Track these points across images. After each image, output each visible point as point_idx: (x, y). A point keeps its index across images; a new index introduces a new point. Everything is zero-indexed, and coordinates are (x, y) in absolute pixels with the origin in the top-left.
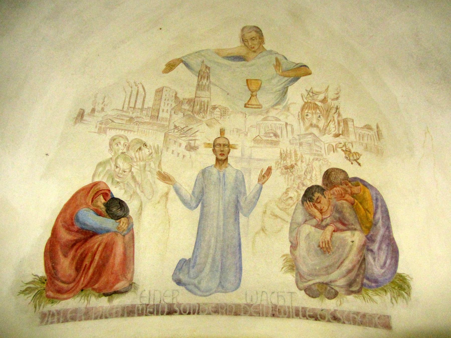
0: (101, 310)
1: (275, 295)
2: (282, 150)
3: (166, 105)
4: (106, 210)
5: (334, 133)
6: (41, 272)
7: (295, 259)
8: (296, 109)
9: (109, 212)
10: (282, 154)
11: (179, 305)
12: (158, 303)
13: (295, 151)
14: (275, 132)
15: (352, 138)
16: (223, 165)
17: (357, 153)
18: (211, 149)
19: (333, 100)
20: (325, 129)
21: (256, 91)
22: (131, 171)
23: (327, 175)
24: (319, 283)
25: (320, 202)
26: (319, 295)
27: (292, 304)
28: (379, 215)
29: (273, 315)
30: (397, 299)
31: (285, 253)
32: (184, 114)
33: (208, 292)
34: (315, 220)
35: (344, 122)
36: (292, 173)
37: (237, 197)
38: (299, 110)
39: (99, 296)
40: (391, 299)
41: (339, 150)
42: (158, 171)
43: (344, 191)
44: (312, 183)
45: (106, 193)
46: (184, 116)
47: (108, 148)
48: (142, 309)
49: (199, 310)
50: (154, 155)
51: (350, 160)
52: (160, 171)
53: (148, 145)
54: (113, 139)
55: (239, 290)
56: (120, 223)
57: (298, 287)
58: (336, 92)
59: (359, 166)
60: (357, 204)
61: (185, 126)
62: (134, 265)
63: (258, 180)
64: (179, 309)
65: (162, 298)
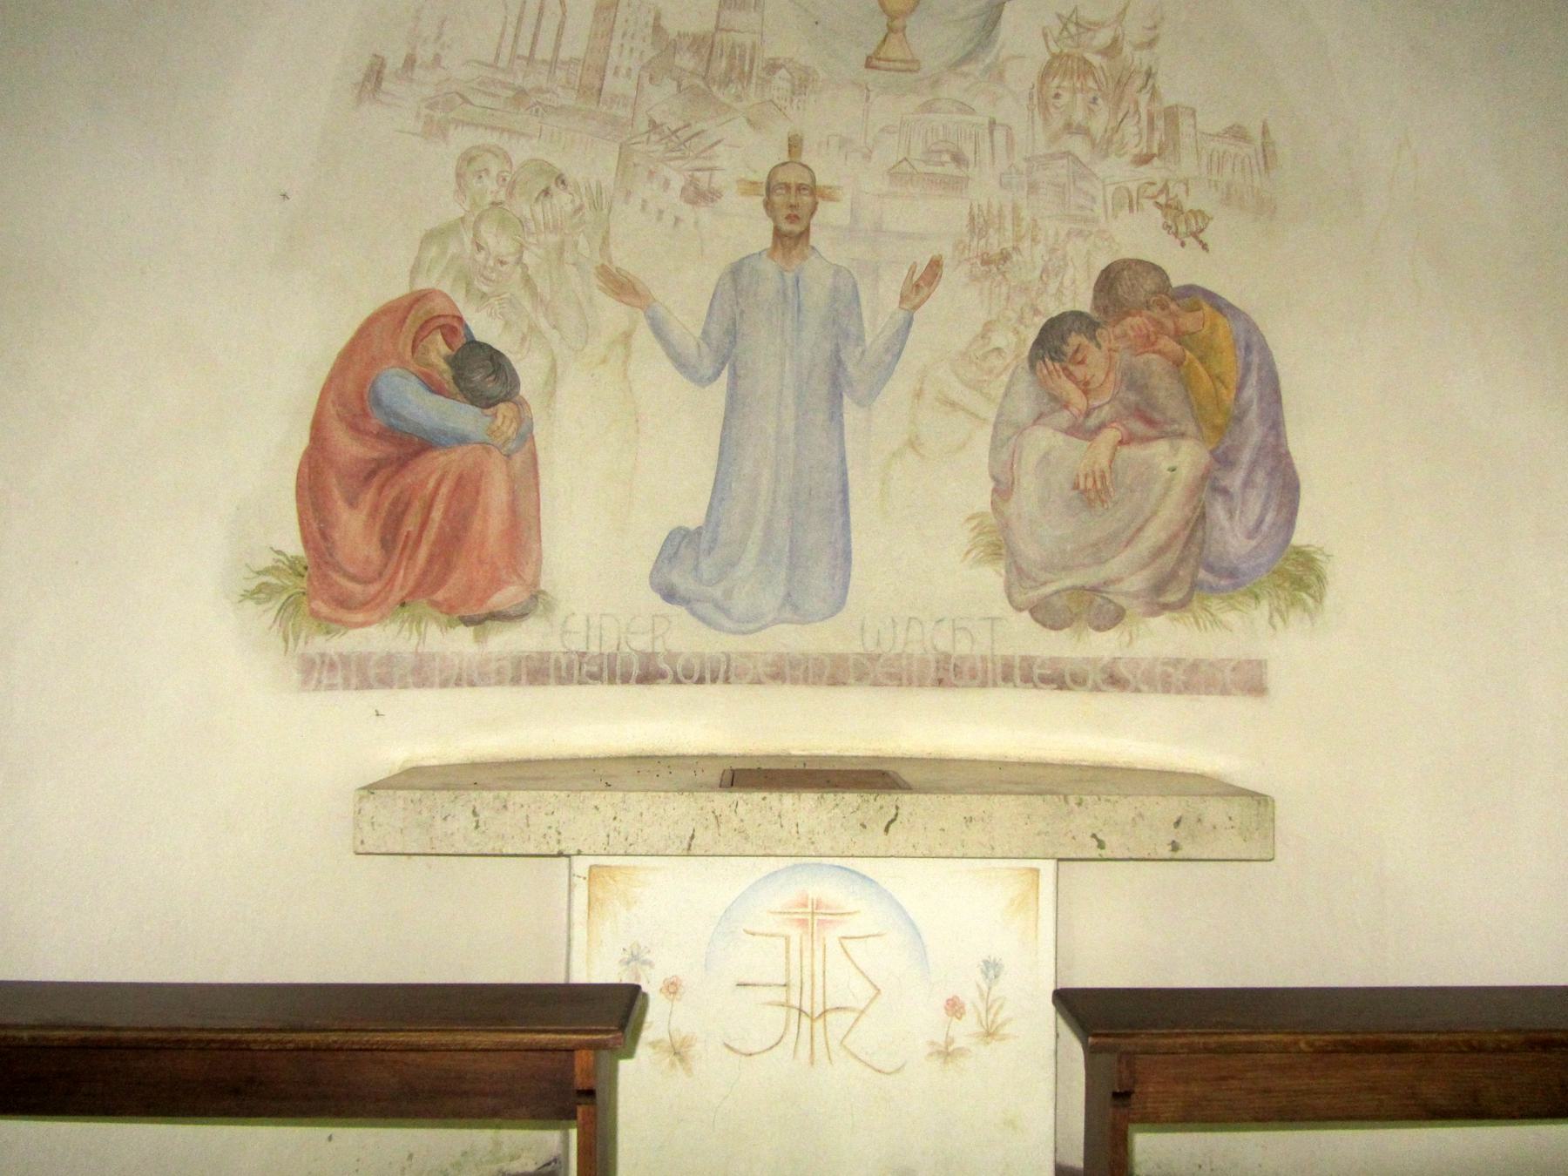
0: (457, 662)
1: (946, 626)
2: (975, 204)
3: (626, 52)
4: (454, 378)
5: (1136, 151)
6: (294, 546)
7: (1005, 527)
8: (1023, 75)
9: (462, 384)
10: (976, 217)
11: (671, 657)
12: (614, 649)
13: (1015, 209)
14: (956, 150)
15: (1188, 165)
16: (794, 252)
17: (1199, 211)
18: (759, 200)
19: (1139, 47)
20: (1110, 141)
21: (905, 14)
22: (519, 261)
23: (1108, 281)
24: (1074, 588)
25: (1082, 362)
26: (1072, 620)
27: (992, 649)
28: (1251, 392)
29: (940, 682)
30: (1288, 618)
31: (976, 510)
32: (679, 86)
33: (751, 623)
34: (1066, 413)
35: (1166, 117)
36: (1004, 276)
37: (837, 351)
38: (1034, 78)
39: (451, 625)
40: (1271, 616)
41: (1148, 204)
42: (599, 265)
43: (1153, 326)
44: (1063, 304)
45: (452, 327)
46: (680, 91)
47: (454, 186)
48: (569, 667)
49: (727, 671)
50: (588, 215)
51: (1176, 234)
52: (606, 263)
53: (569, 180)
54: (468, 158)
55: (842, 616)
56: (496, 417)
57: (1011, 602)
58: (1149, 23)
59: (1204, 252)
60: (1191, 362)
61: (681, 124)
62: (541, 541)
63: (901, 297)
64: (672, 668)
65: (623, 641)
